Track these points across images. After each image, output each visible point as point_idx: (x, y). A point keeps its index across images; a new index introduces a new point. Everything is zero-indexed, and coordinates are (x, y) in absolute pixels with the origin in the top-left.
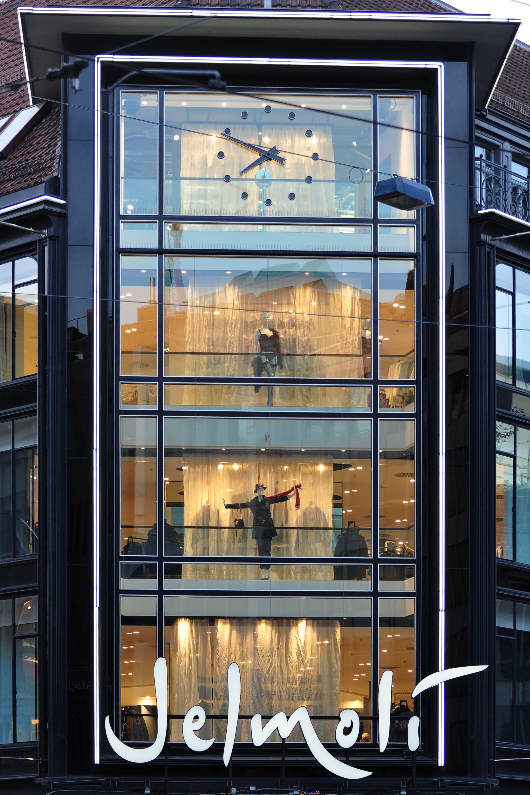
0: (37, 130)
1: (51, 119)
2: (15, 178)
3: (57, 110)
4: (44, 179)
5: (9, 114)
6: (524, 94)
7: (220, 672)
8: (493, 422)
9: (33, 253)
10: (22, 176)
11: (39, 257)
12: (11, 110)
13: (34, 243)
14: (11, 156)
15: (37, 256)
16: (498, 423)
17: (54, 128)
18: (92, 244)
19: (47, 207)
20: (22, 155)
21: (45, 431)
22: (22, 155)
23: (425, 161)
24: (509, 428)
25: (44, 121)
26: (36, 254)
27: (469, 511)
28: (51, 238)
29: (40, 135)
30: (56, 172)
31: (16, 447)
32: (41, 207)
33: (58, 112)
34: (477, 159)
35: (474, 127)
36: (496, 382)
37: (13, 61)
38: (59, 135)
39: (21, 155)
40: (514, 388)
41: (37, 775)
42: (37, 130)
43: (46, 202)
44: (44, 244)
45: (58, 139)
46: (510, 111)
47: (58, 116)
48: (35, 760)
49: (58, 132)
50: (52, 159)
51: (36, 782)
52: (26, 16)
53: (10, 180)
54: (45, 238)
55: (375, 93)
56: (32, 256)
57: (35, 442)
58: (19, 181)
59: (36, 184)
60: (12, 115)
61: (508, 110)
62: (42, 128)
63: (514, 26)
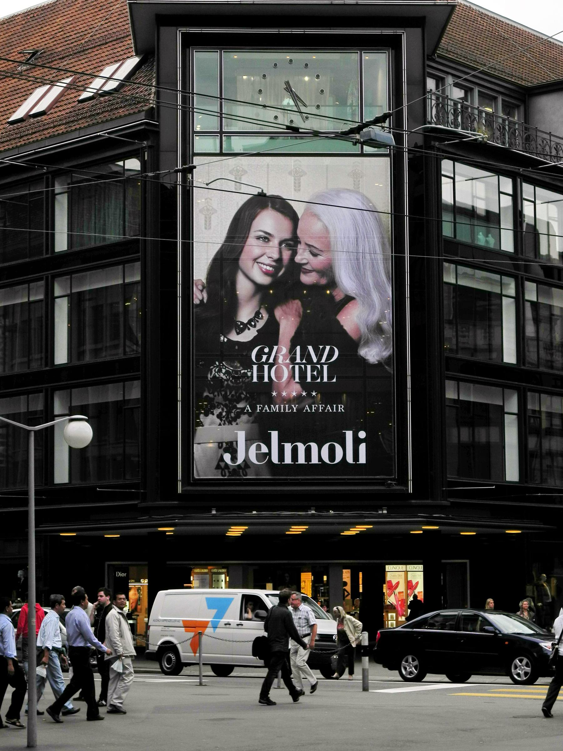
0: (139, 73)
1: (148, 66)
2: (125, 106)
3: (151, 60)
4: (144, 108)
5: (119, 60)
6: (462, 39)
7: (91, 216)
8: (441, 263)
9: (138, 156)
10: (130, 105)
11: (141, 158)
12: (120, 58)
13: (138, 149)
14: (122, 91)
15: (140, 158)
16: (444, 263)
17: (150, 73)
18: (175, 150)
19: (146, 127)
20: (129, 90)
21: (145, 272)
22: (129, 90)
23: (394, 94)
24: (453, 266)
25: (143, 67)
26: (139, 156)
27: (96, 526)
28: (150, 147)
29: (141, 77)
30: (152, 104)
31: (127, 281)
32: (142, 127)
33: (152, 61)
34: (428, 92)
35: (426, 73)
36: (443, 237)
37: (121, 22)
38: (154, 78)
39: (128, 90)
40: (455, 240)
41: (139, 501)
42: (139, 73)
43: (146, 123)
44: (145, 150)
45: (153, 81)
46: (452, 54)
47: (153, 64)
48: (58, 534)
49: (153, 75)
50: (149, 94)
51: (138, 506)
52: (132, 5)
53: (121, 107)
54: (145, 147)
55: (361, 50)
56: (137, 158)
57: (138, 278)
58: (127, 109)
59: (139, 112)
60: (121, 62)
61: (450, 53)
62: (142, 72)
63: (450, 8)
